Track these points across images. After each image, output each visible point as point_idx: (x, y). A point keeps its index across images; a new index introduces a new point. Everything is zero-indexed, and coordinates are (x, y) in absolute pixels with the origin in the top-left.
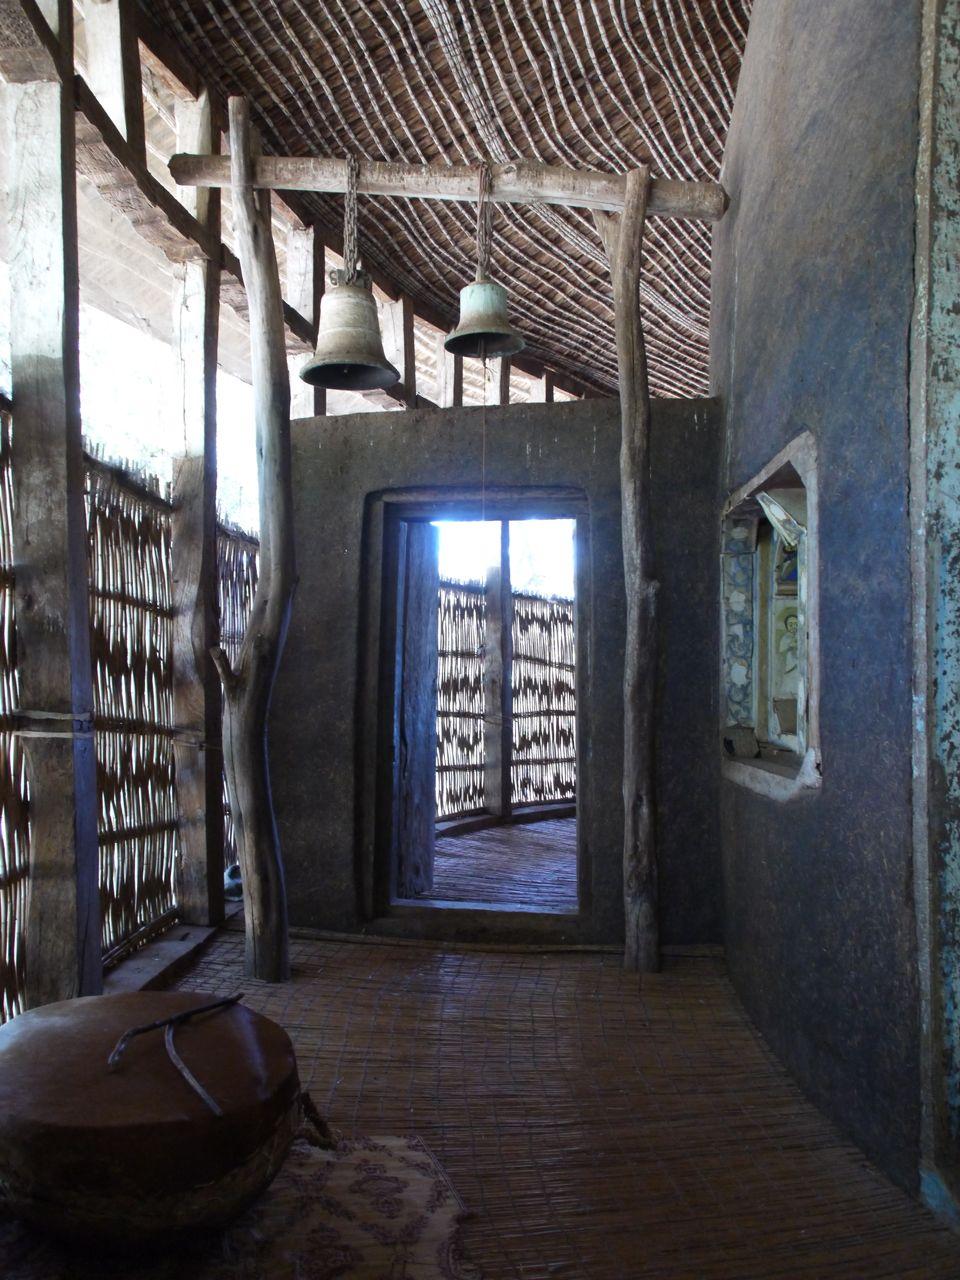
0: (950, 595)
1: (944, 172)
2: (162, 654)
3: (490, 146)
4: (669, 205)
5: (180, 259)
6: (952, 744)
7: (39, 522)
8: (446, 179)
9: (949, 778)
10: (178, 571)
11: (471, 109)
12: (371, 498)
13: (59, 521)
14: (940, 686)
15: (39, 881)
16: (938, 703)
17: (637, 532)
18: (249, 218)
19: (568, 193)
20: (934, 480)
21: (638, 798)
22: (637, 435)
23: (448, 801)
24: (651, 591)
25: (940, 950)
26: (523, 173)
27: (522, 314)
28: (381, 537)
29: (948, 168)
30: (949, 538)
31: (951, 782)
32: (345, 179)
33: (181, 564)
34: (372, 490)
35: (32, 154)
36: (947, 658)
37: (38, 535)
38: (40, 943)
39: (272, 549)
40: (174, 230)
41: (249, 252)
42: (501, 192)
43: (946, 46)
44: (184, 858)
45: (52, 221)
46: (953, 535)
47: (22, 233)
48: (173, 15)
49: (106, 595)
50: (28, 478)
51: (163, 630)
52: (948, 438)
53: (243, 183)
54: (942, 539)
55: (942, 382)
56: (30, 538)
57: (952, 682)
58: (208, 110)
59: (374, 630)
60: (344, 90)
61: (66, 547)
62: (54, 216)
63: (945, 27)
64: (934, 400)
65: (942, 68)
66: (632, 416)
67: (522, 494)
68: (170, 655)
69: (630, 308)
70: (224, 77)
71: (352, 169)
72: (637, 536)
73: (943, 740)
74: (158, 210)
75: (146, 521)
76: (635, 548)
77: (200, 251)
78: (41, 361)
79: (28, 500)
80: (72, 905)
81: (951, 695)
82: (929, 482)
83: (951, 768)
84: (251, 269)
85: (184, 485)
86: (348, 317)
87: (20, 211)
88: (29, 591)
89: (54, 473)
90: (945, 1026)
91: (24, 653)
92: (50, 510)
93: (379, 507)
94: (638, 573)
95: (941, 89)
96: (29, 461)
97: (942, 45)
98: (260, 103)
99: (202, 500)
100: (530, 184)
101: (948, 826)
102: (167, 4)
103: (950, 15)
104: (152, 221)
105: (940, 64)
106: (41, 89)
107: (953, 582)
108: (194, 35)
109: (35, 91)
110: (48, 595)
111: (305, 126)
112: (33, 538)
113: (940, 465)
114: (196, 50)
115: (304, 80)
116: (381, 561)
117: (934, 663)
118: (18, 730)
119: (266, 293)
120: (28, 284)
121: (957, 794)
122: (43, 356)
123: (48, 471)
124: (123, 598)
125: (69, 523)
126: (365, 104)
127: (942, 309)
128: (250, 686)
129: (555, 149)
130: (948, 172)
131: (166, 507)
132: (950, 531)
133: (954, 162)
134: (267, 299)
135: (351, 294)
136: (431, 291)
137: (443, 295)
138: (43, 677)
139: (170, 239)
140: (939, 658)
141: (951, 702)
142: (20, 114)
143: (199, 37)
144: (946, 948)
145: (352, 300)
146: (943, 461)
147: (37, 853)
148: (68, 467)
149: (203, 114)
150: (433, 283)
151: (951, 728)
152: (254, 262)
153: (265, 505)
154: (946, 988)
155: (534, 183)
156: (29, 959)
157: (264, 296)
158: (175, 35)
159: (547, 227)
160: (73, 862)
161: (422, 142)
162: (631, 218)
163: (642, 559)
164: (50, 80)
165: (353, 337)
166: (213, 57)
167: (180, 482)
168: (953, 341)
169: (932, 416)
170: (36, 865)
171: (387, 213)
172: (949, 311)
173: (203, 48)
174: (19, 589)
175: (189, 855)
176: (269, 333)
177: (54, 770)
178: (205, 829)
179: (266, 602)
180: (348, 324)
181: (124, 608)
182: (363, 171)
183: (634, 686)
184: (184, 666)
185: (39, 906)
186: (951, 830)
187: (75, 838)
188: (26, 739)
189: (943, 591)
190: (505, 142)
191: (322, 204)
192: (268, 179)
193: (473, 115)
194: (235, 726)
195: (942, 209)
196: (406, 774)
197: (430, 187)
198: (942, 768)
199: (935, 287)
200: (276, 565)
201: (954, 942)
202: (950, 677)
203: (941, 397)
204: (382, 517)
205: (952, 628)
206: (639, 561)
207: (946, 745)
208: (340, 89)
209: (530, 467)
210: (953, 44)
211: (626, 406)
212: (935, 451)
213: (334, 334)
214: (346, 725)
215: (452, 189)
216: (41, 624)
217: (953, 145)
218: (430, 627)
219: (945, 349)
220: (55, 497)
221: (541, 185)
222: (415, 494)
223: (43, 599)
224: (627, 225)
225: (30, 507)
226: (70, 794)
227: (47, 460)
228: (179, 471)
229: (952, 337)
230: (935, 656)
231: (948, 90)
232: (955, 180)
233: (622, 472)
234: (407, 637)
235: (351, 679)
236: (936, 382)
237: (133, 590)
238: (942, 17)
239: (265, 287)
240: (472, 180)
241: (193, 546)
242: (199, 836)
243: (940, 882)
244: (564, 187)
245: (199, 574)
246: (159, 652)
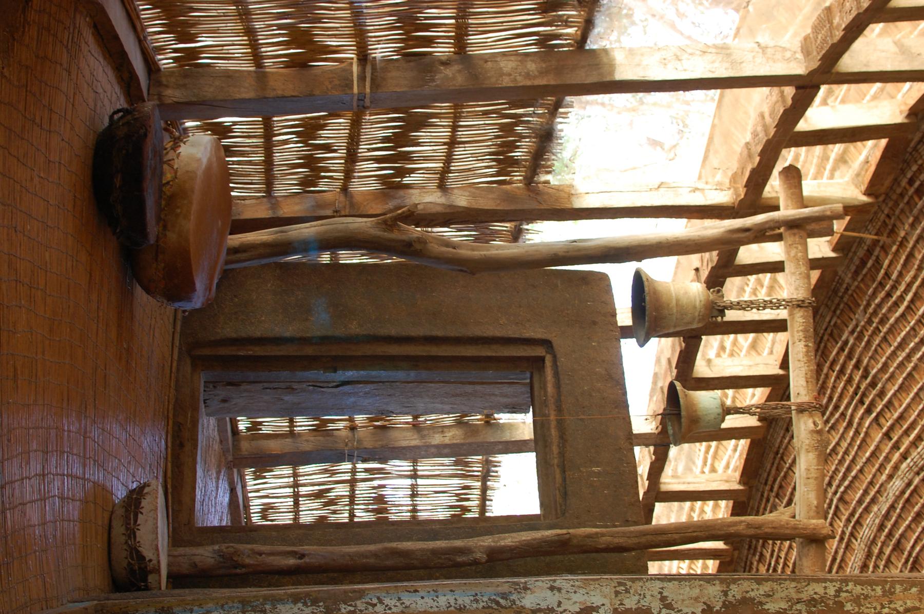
0: (474, 600)
1: (752, 587)
2: (407, 180)
4: (804, 560)
5: (732, 184)
6: (375, 605)
7: (501, 68)
8: (803, 375)
9: (353, 603)
11: (919, 450)
12: (546, 344)
14: (414, 594)
16: (403, 594)
17: (528, 540)
18: (756, 225)
19: (804, 474)
20: (549, 586)
21: (302, 556)
22: (609, 539)
23: (264, 504)
24: (478, 555)
25: (239, 602)
26: (815, 435)
28: (515, 354)
29: (755, 590)
31: (351, 605)
33: (483, 193)
34: (554, 345)
35: (754, 57)
36: (433, 599)
37: (492, 68)
39: (497, 252)
40: (747, 174)
41: (729, 226)
43: (835, 586)
44: (242, 202)
47: (698, 52)
48: (915, 168)
49: (455, 128)
50: (531, 61)
52: (578, 595)
53: (783, 219)
54: (510, 592)
55: (614, 589)
56: (489, 63)
57: (417, 604)
58: (856, 203)
59: (435, 351)
61: (484, 86)
62: (713, 72)
63: (847, 585)
65: (820, 584)
66: (624, 534)
68: (408, 186)
70: (888, 216)
71: (803, 301)
72: (524, 540)
73: (378, 598)
75: (515, 162)
76: (514, 540)
77: (739, 199)
78: (612, 67)
79: (516, 61)
80: (238, 96)
81: (408, 603)
83: (360, 605)
84: (716, 228)
85: (548, 194)
86: (684, 301)
87: (714, 50)
89: (535, 77)
91: (410, 61)
92: (510, 75)
93: (539, 351)
94: (493, 544)
95: (806, 583)
96: (543, 60)
97: (834, 584)
98: (880, 252)
100: (807, 442)
101: (321, 604)
102: (920, 162)
105: (822, 582)
106: (799, 62)
107: (483, 602)
108: (907, 187)
109: (797, 58)
111: (874, 295)
112: (490, 65)
113: (559, 590)
114: (899, 191)
115: (902, 287)
116: (494, 355)
117: (429, 590)
119: (698, 240)
121: (343, 611)
122: (615, 68)
123: (536, 73)
124: (452, 143)
125: (501, 88)
126: (901, 346)
127: (662, 588)
128: (387, 235)
130: (753, 590)
131: (529, 180)
132: (516, 599)
133: (760, 595)
134: (694, 241)
135: (703, 303)
136: (775, 458)
137: (773, 471)
139: (742, 173)
140: (432, 593)
141: (403, 603)
142: (780, 49)
143: (907, 190)
144: (240, 606)
145: (698, 303)
146: (562, 591)
147: (272, 73)
148: (539, 86)
150: (782, 458)
151: (386, 604)
152: (722, 230)
153: (531, 246)
154: (214, 608)
155: (809, 445)
156: (200, 70)
158: (903, 172)
159: (847, 565)
160: (267, 96)
161: (886, 410)
162: (787, 524)
163: (504, 547)
165: (668, 305)
166: (899, 205)
167: (551, 191)
169: (591, 583)
171: (829, 392)
172: (661, 593)
173: (902, 195)
175: (244, 205)
176: (668, 243)
177: (330, 82)
179: (454, 248)
180: (678, 300)
181: (445, 144)
182: (803, 310)
183: (396, 548)
184: (400, 197)
187: (284, 97)
188: (351, 64)
189: (476, 594)
190: (903, 492)
191: (824, 327)
192: (789, 239)
193: (915, 454)
195: (728, 587)
197: (797, 362)
198: (360, 598)
199: (676, 583)
200: (485, 255)
201: (244, 612)
203: (604, 588)
205: (452, 602)
206: (503, 544)
207: (375, 601)
209: (581, 471)
210: (836, 591)
211: (632, 530)
212: (568, 585)
214: (354, 328)
215: (797, 381)
216: (430, 72)
217: (771, 593)
218: (440, 406)
219: (636, 591)
220: (519, 78)
221: (808, 451)
223: (449, 72)
224: (781, 521)
225: (511, 62)
226: (314, 93)
227: (543, 73)
228: (558, 189)
229: (645, 597)
230: (433, 590)
231: (806, 589)
232: (748, 595)
233: (577, 529)
235: (393, 332)
237: (459, 151)
239: (703, 238)
240: (806, 395)
242: (263, 213)
243: (284, 600)
244: (808, 470)
245: (476, 207)
246: (410, 177)
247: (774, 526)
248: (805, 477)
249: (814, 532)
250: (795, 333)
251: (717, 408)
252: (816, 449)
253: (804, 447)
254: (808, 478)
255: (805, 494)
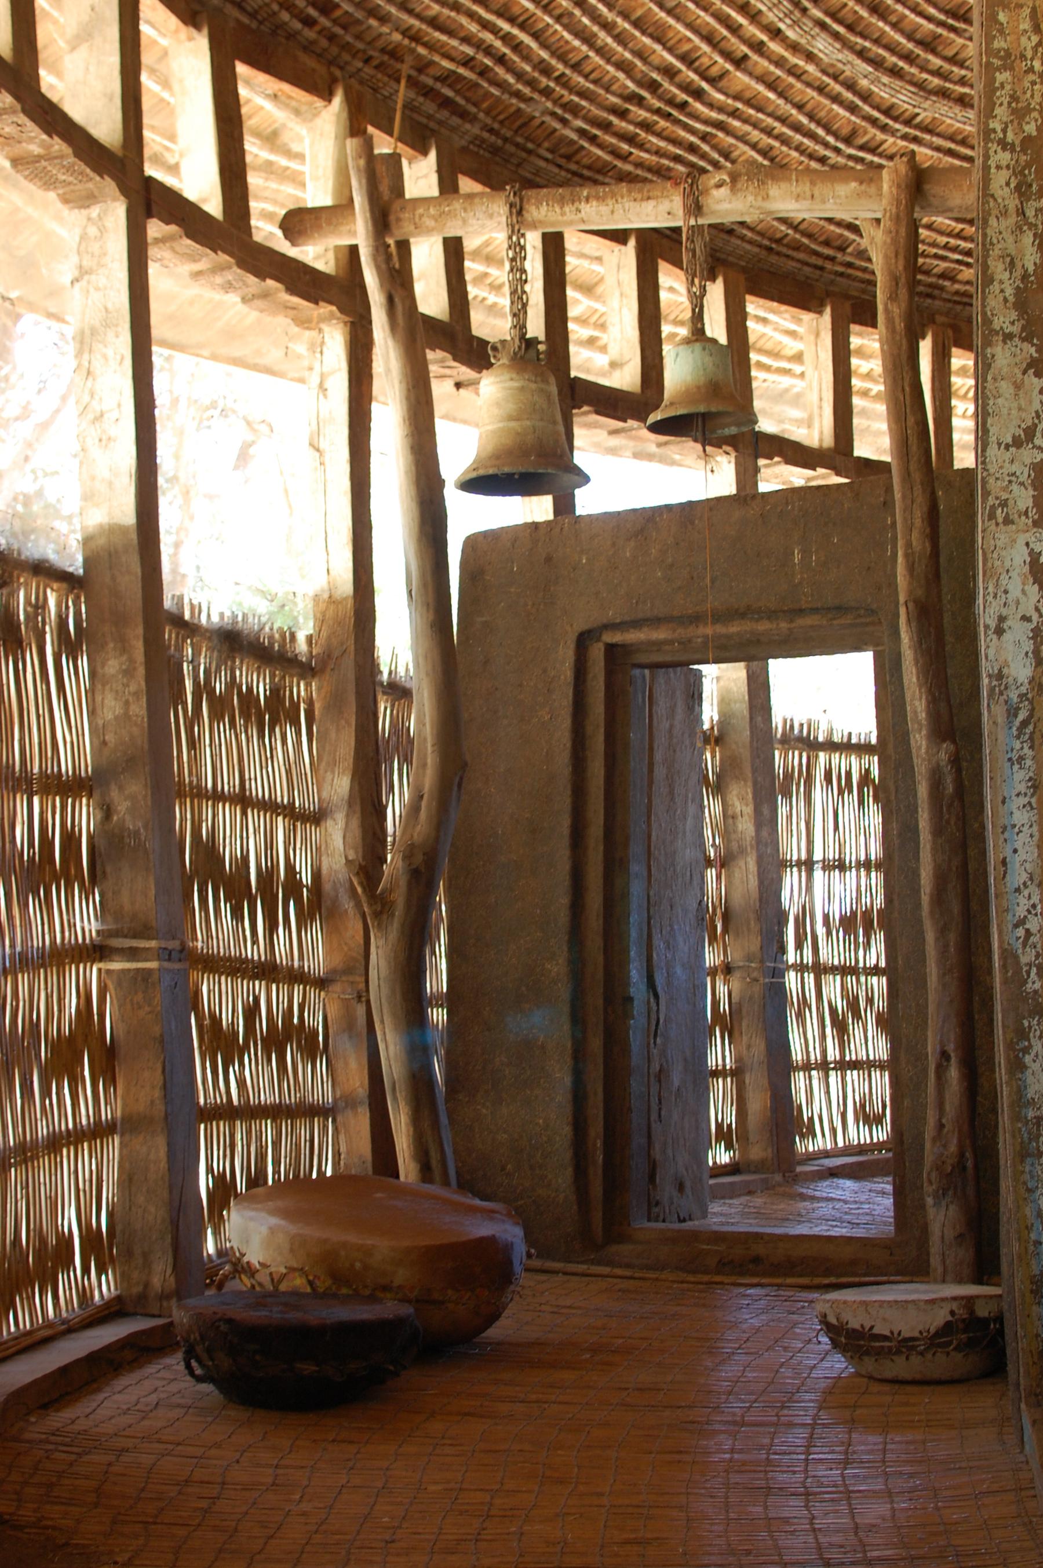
1: (997, 291)
2: (306, 878)
3: (813, 47)
6: (1027, 931)
7: (116, 718)
8: (637, 205)
9: (1025, 969)
10: (325, 758)
11: (764, 8)
12: (583, 641)
13: (137, 715)
15: (127, 1137)
18: (382, 285)
19: (805, 204)
20: (995, 637)
21: (945, 1055)
22: (915, 535)
24: (943, 756)
25: (1022, 1162)
26: (739, 185)
27: (958, 262)
28: (601, 694)
29: (1003, 286)
30: (1015, 700)
31: (1028, 973)
32: (504, 219)
35: (97, 289)
36: (1018, 834)
37: (116, 733)
38: (130, 1209)
41: (384, 331)
42: (712, 213)
45: (121, 363)
46: (1020, 696)
47: (89, 383)
48: (285, 16)
50: (103, 666)
51: (304, 840)
52: (1010, 587)
53: (371, 240)
54: (1006, 702)
56: (107, 738)
57: (1025, 861)
58: (345, 115)
60: (551, 31)
61: (146, 747)
62: (122, 358)
63: (994, 131)
64: (992, 548)
66: (908, 509)
67: (791, 621)
68: (317, 875)
69: (899, 355)
70: (367, 61)
72: (918, 678)
73: (1016, 926)
74: (270, 283)
75: (276, 694)
77: (338, 314)
78: (113, 530)
80: (163, 1164)
81: (1024, 876)
82: (988, 639)
83: (1027, 957)
84: (388, 353)
85: (329, 638)
86: (511, 407)
87: (86, 356)
88: (107, 799)
89: (131, 660)
90: (1032, 1248)
91: (104, 872)
92: (127, 703)
93: (597, 653)
94: (924, 732)
95: (991, 200)
97: (991, 153)
98: (427, 75)
99: (352, 656)
100: (750, 198)
101: (1026, 1023)
102: (275, 7)
103: (998, 118)
104: (265, 295)
106: (105, 212)
107: (1022, 748)
109: (99, 215)
110: (128, 803)
111: (501, 85)
112: (110, 737)
113: (1002, 619)
114: (324, 43)
115: (488, 37)
116: (602, 730)
117: (1001, 840)
118: (100, 960)
119: (408, 383)
120: (97, 441)
121: (1037, 986)
122: (116, 524)
123: (124, 658)
124: (243, 800)
125: (149, 717)
126: (588, 39)
127: (999, 444)
128: (399, 910)
129: (931, 26)
130: (1002, 291)
131: (306, 670)
132: (1017, 692)
134: (409, 390)
135: (514, 376)
136: (778, 254)
137: (801, 256)
138: (125, 899)
139: (294, 308)
140: (1006, 835)
141: (1025, 884)
142: (84, 245)
143: (324, 29)
144: (1029, 1160)
145: (516, 384)
146: (1004, 614)
147: (125, 1106)
149: (338, 122)
150: (779, 241)
152: (391, 343)
156: (119, 1228)
157: (404, 385)
158: (292, 36)
159: (959, 131)
160: (163, 1114)
161: (697, 64)
162: (891, 232)
164: (114, 200)
168: (1013, 479)
169: (989, 565)
170: (123, 1118)
172: (1007, 447)
173: (332, 38)
174: (97, 794)
175: (348, 1153)
176: (413, 435)
177: (140, 1008)
178: (368, 1114)
179: (422, 797)
181: (244, 813)
182: (526, 206)
184: (335, 889)
185: (127, 1165)
186: (1030, 1027)
188: (108, 971)
189: (1010, 759)
190: (836, 36)
191: (556, 170)
193: (770, 14)
194: (383, 963)
195: (997, 333)
196: (658, 1040)
197: (616, 216)
198: (1016, 957)
199: (989, 421)
201: (1040, 1154)
202: (1022, 855)
203: (999, 544)
204: (602, 664)
206: (924, 715)
207: (1021, 932)
208: (547, 30)
209: (800, 583)
210: (1004, 149)
212: (994, 604)
213: (493, 432)
214: (557, 967)
215: (647, 215)
217: (1008, 259)
218: (690, 822)
220: (133, 688)
221: (767, 197)
222: (645, 629)
223: (122, 808)
224: (885, 243)
225: (106, 701)
226: (158, 1035)
227: (124, 647)
228: (321, 621)
229: (1014, 474)
230: (1003, 833)
231: (1000, 200)
232: (1011, 299)
234: (654, 838)
235: (565, 901)
236: (993, 527)
237: (257, 789)
238: (991, 121)
240: (671, 201)
241: (343, 722)
243: (1019, 1087)
244: (798, 197)
245: (352, 760)
247: (893, 255)
248: (810, 202)
249: (903, 187)
250: (565, 218)
251: (692, 352)
252: (763, 183)
253: (760, 203)
254: (813, 196)
255: (838, 201)
